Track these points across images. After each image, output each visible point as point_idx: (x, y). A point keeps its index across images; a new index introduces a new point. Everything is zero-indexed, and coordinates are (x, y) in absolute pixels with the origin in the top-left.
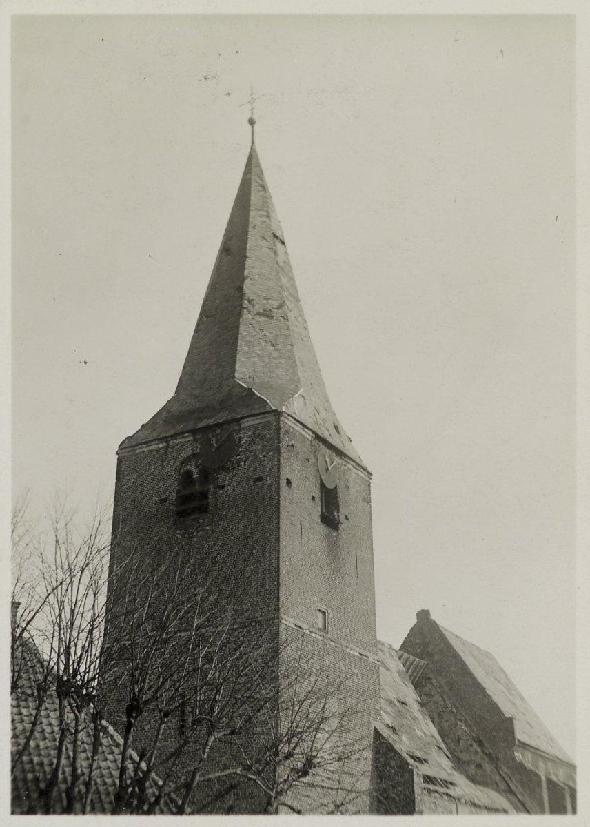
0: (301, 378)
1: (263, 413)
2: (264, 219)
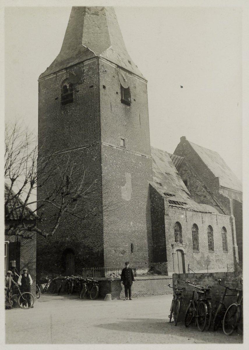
0: (111, 41)
1: (92, 58)
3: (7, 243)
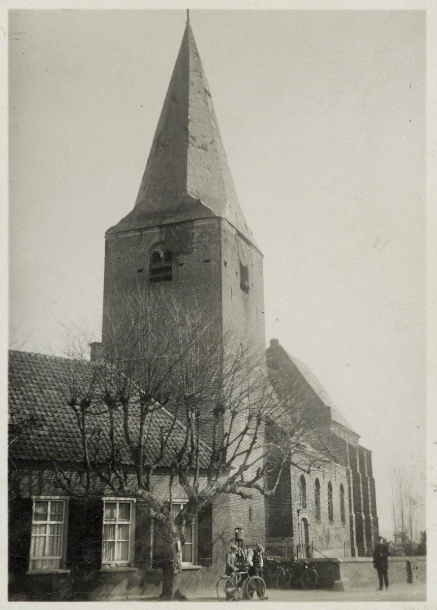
2: (198, 78)
3: (133, 501)
